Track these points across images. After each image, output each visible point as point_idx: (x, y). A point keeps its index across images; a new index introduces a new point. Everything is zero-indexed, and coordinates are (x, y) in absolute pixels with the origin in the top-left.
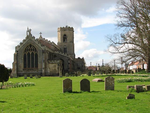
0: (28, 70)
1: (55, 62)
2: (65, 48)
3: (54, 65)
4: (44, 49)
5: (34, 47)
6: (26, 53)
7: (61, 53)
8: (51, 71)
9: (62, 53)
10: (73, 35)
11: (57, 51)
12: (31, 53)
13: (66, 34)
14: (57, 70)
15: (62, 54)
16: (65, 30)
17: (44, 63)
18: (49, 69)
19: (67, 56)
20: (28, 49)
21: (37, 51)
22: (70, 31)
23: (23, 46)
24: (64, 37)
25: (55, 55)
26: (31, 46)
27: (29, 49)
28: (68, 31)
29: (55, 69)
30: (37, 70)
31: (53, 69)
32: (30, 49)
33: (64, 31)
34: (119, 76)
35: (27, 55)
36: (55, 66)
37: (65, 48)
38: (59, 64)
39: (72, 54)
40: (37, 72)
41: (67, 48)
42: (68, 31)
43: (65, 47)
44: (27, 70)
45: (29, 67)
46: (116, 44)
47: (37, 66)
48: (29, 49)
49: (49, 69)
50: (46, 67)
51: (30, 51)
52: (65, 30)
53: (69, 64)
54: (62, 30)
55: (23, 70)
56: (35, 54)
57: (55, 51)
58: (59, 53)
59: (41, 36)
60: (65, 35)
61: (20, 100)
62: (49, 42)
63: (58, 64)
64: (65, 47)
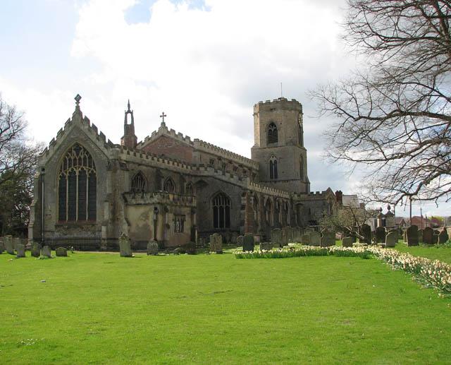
0: (68, 228)
1: (147, 202)
3: (142, 210)
4: (113, 157)
5: (87, 153)
6: (66, 172)
7: (219, 175)
8: (133, 230)
9: (224, 174)
10: (301, 128)
11: (208, 169)
12: (77, 174)
13: (274, 122)
14: (152, 227)
15: (224, 178)
16: (271, 110)
17: (107, 203)
18: (126, 227)
19: (238, 184)
20: (70, 160)
21: (94, 165)
22: (288, 111)
23: (56, 152)
24: (270, 130)
25: (200, 182)
26: (78, 148)
27: (72, 158)
28: (279, 111)
29: (146, 226)
31: (140, 226)
33: (271, 113)
34: (345, 256)
35: (67, 178)
36: (146, 216)
38: (158, 206)
41: (278, 161)
42: (279, 111)
43: (273, 160)
44: (64, 229)
45: (72, 217)
46: (356, 120)
47: (93, 217)
48: (72, 158)
49: (127, 224)
50: (114, 219)
52: (271, 110)
53: (243, 207)
54: (265, 109)
55: (57, 226)
56: (88, 176)
57: (202, 169)
58: (216, 174)
59: (163, 124)
60: (272, 124)
61: (434, 273)
62: (187, 142)
63: (156, 209)
64: (273, 160)
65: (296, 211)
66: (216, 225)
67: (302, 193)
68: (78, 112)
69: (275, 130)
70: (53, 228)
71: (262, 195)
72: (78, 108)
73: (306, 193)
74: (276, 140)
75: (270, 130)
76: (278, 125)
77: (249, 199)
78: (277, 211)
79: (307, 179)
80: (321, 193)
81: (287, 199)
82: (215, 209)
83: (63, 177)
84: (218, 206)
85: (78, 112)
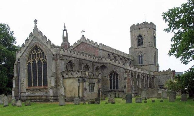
1: (74, 76)
2: (140, 55)
3: (71, 81)
5: (42, 51)
6: (31, 61)
10: (155, 38)
11: (107, 59)
12: (37, 62)
15: (115, 64)
16: (139, 29)
19: (123, 67)
20: (33, 55)
24: (139, 39)
26: (36, 48)
27: (39, 53)
30: (46, 91)
32: (35, 54)
35: (31, 64)
37: (140, 55)
39: (151, 65)
40: (46, 94)
43: (140, 54)
47: (46, 84)
48: (39, 53)
50: (57, 85)
51: (36, 57)
52: (139, 29)
53: (125, 79)
56: (42, 63)
57: (104, 59)
58: (111, 62)
59: (83, 36)
60: (140, 36)
62: (95, 45)
64: (140, 54)
65: (152, 81)
66: (111, 88)
67: (155, 71)
68: (36, 29)
69: (142, 39)
70: (25, 91)
71: (135, 72)
72: (36, 26)
73: (157, 71)
74: (142, 44)
75: (139, 39)
76: (143, 36)
77: (128, 75)
78: (143, 81)
79: (158, 64)
80: (165, 71)
81: (147, 74)
82: (111, 80)
83: (29, 64)
84: (112, 79)
85: (36, 29)
